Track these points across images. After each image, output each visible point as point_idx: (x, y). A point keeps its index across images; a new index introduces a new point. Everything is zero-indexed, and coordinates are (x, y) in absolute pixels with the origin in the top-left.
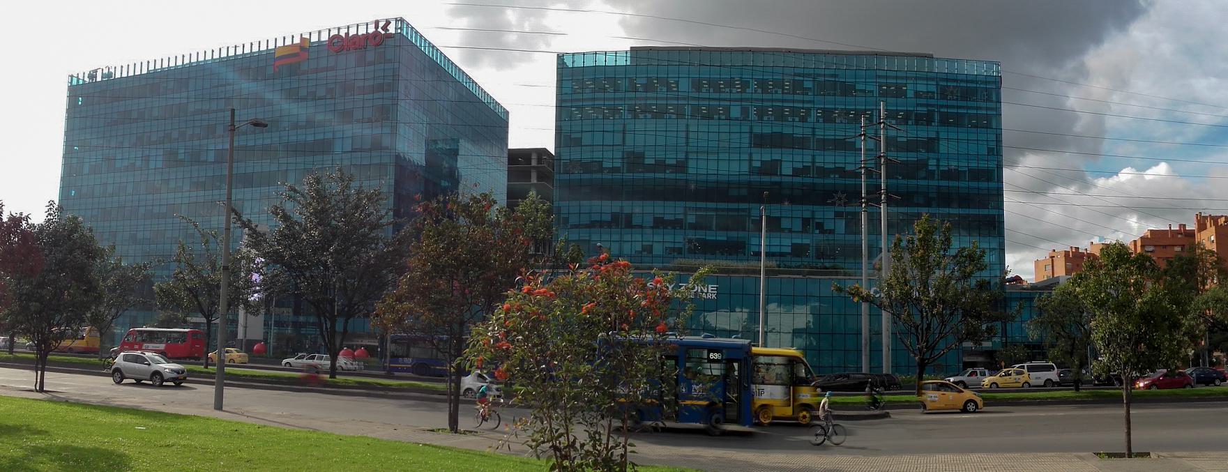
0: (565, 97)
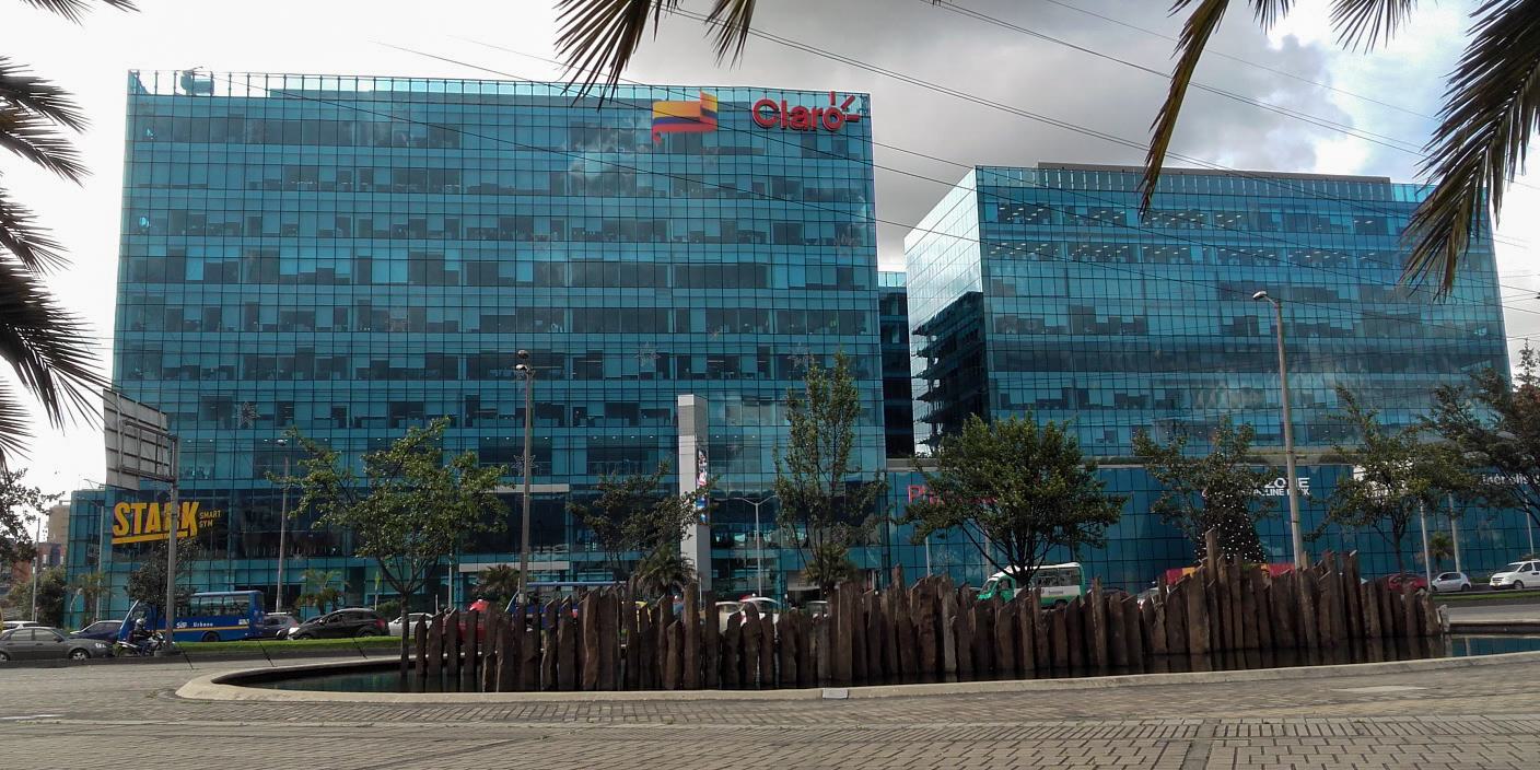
0: (990, 227)
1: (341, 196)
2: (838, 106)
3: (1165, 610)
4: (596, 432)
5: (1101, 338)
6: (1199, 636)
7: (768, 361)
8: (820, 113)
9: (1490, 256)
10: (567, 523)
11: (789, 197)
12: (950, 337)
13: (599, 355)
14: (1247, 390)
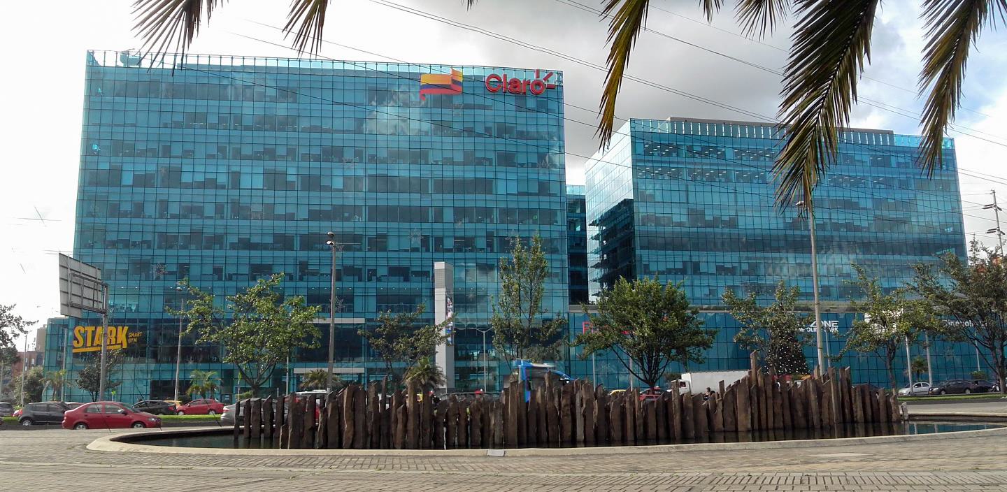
0: (639, 158)
1: (221, 132)
2: (541, 78)
3: (723, 403)
4: (382, 285)
5: (708, 230)
6: (744, 420)
7: (493, 240)
8: (528, 83)
9: (956, 181)
10: (363, 343)
11: (507, 136)
12: (612, 227)
13: (385, 236)
14: (800, 264)
